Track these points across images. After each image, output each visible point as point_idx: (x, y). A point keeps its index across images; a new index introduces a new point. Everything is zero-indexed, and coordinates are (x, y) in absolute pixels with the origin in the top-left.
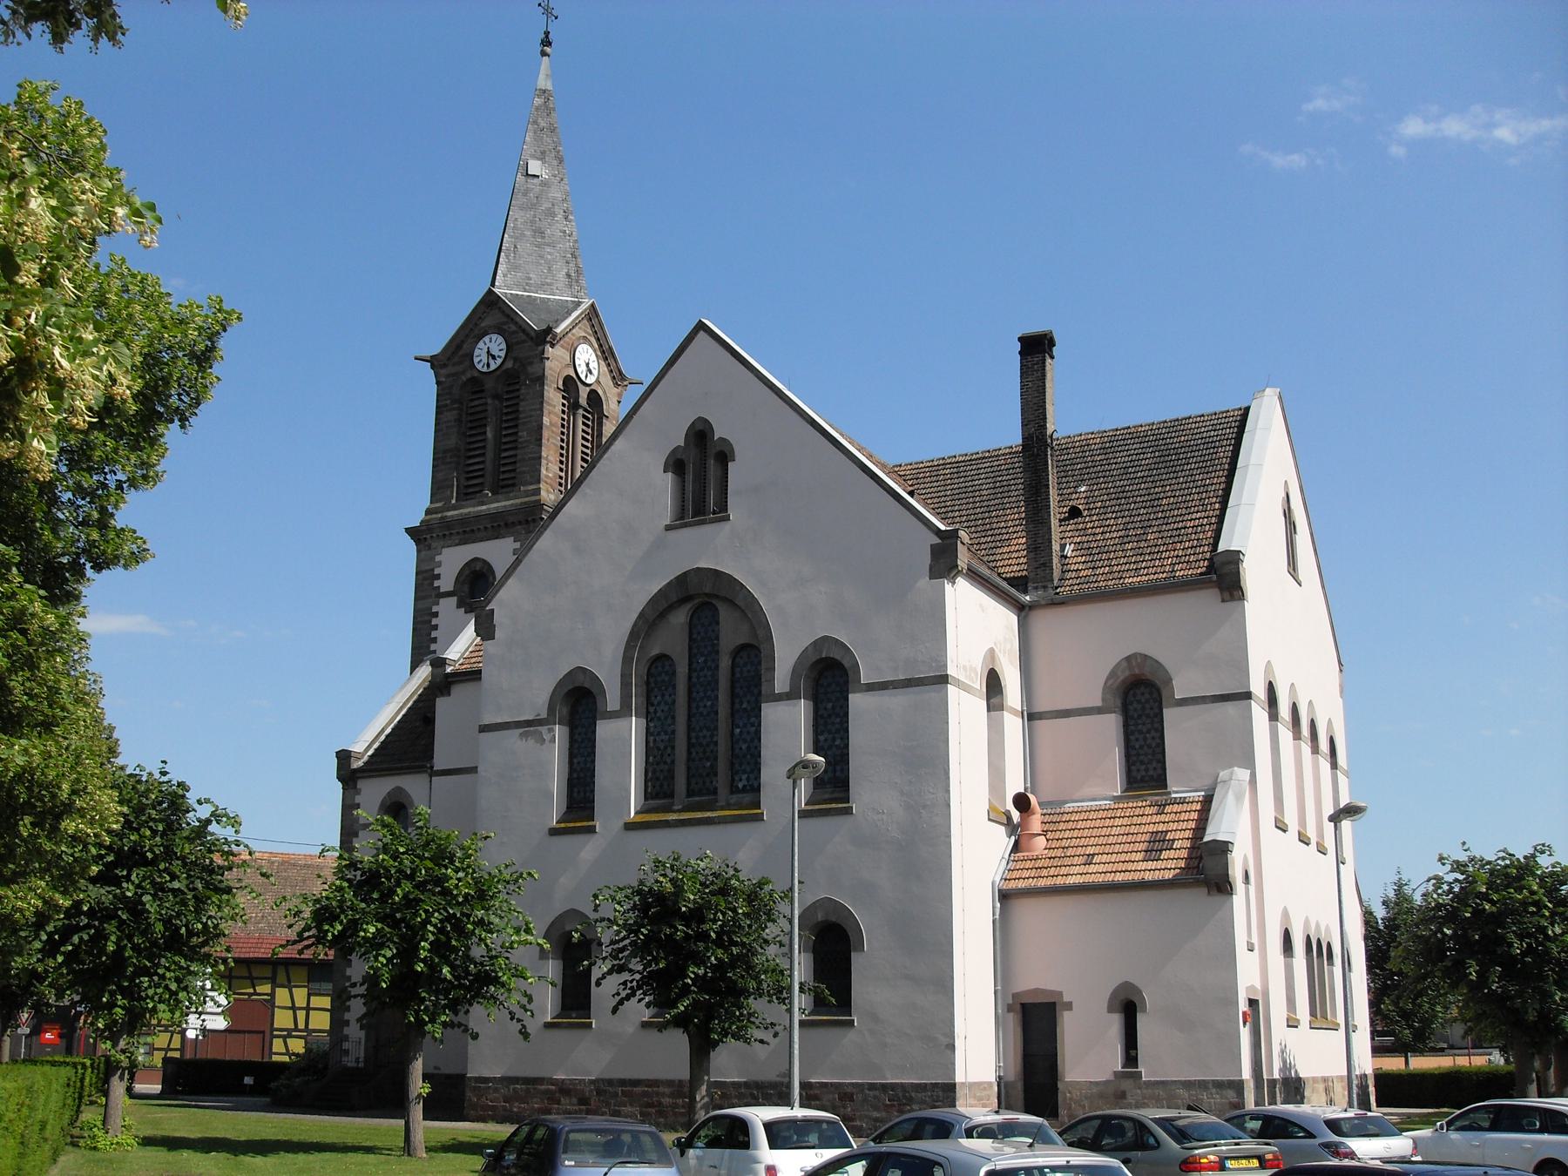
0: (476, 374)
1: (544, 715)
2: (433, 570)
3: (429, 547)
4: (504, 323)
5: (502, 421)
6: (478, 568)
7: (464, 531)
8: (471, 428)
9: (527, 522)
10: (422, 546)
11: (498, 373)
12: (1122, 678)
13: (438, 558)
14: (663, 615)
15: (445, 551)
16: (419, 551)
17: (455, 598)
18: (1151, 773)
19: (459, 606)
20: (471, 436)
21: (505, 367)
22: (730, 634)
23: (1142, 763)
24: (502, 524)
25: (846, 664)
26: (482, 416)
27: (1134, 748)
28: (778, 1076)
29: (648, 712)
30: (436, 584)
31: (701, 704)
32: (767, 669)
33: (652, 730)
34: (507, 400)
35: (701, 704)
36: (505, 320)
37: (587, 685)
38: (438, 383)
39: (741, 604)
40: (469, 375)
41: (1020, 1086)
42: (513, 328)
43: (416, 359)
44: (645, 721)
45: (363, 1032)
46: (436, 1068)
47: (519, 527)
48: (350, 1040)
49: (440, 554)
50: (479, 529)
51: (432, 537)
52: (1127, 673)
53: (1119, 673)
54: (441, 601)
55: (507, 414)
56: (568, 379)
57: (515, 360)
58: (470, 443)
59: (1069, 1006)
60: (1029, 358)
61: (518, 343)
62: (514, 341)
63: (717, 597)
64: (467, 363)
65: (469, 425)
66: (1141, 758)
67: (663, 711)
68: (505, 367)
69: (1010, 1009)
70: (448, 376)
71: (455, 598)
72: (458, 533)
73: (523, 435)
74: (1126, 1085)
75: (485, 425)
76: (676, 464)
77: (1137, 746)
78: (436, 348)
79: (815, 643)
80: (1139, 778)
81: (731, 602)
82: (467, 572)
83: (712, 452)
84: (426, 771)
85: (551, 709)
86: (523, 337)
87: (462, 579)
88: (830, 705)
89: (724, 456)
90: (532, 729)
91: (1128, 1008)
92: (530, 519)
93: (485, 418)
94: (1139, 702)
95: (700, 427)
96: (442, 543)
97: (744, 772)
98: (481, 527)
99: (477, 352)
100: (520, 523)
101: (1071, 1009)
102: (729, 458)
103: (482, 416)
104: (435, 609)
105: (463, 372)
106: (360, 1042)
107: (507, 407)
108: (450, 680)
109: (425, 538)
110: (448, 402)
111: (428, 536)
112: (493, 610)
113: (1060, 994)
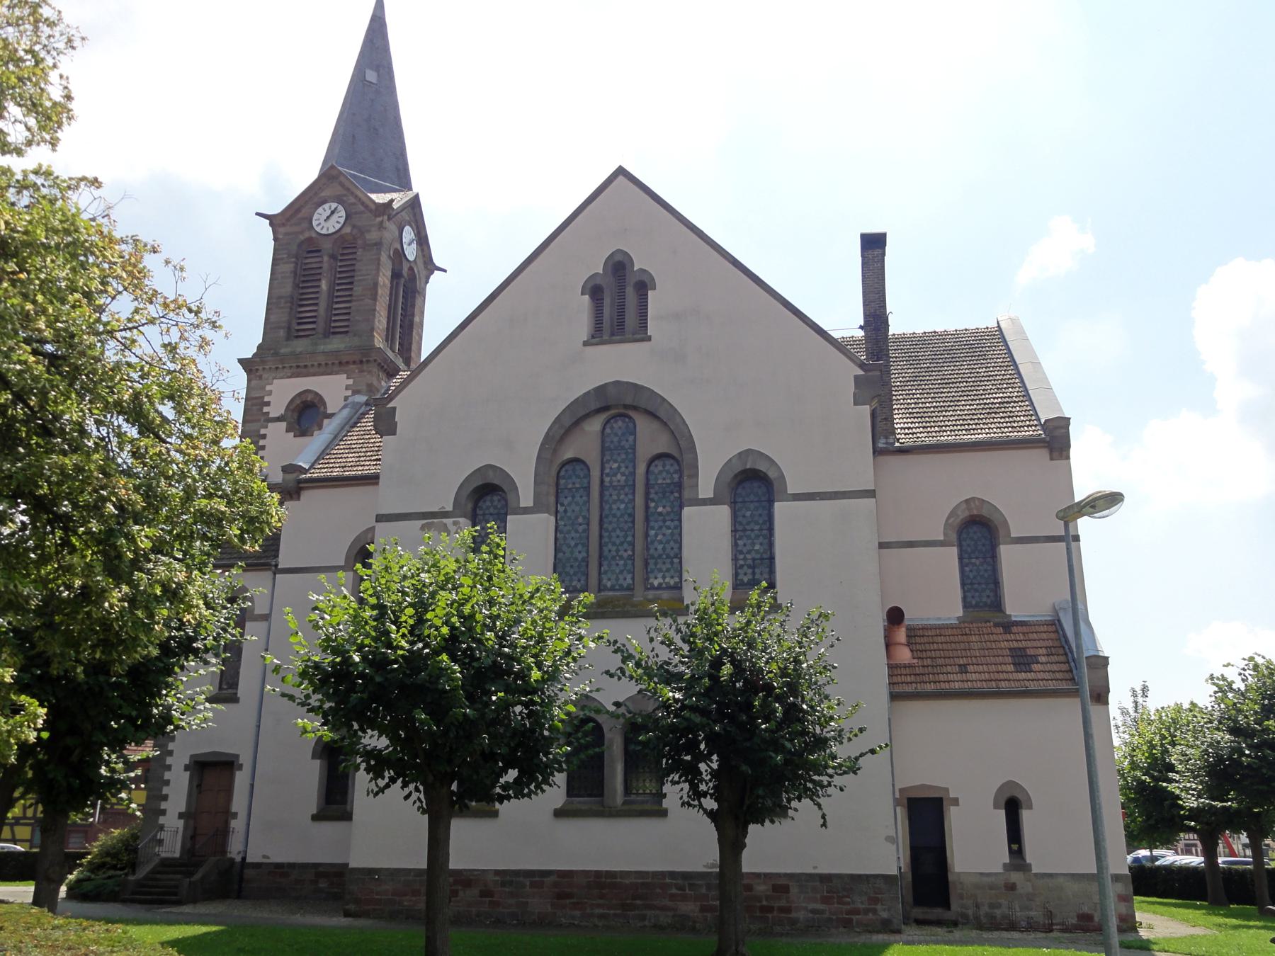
0: (314, 235)
1: (449, 508)
2: (263, 397)
3: (260, 377)
4: (345, 195)
5: (335, 277)
6: (309, 399)
7: (298, 367)
8: (304, 282)
9: (361, 362)
10: (252, 376)
11: (336, 236)
12: (961, 517)
13: (268, 388)
14: (577, 423)
15: (275, 381)
16: (249, 381)
17: (285, 423)
18: (984, 599)
19: (287, 431)
20: (303, 288)
21: (343, 232)
22: (649, 440)
23: (976, 590)
24: (337, 362)
25: (772, 474)
26: (318, 271)
27: (968, 577)
28: (704, 866)
29: (557, 512)
30: (265, 409)
31: (614, 507)
32: (690, 477)
33: (560, 528)
34: (341, 260)
35: (614, 507)
36: (345, 192)
37: (496, 482)
38: (275, 239)
39: (661, 414)
40: (307, 235)
41: (909, 877)
42: (352, 200)
43: (258, 214)
44: (553, 519)
45: (182, 822)
46: (264, 857)
47: (352, 366)
48: (165, 829)
49: (271, 384)
50: (313, 365)
51: (264, 369)
52: (967, 514)
53: (959, 513)
54: (270, 424)
55: (340, 272)
56: (396, 251)
57: (354, 227)
58: (302, 294)
59: (956, 802)
60: (870, 252)
61: (356, 213)
62: (353, 211)
63: (635, 408)
64: (305, 225)
65: (303, 279)
66: (976, 586)
67: (573, 511)
68: (343, 232)
69: (897, 802)
70: (286, 234)
71: (285, 423)
72: (291, 367)
73: (358, 290)
74: (1016, 877)
75: (320, 280)
76: (595, 291)
77: (971, 577)
78: (276, 209)
79: (740, 454)
80: (974, 602)
81: (653, 415)
82: (298, 402)
83: (631, 280)
84: (270, 569)
85: (456, 503)
86: (362, 208)
87: (291, 407)
88: (748, 514)
89: (644, 286)
90: (435, 521)
91: (1013, 807)
92: (364, 360)
93: (320, 274)
94: (972, 539)
95: (618, 258)
96: (274, 375)
97: (660, 570)
98: (316, 364)
99: (316, 216)
100: (354, 362)
101: (958, 805)
102: (649, 287)
103: (318, 271)
104: (263, 432)
105: (302, 232)
106: (177, 832)
107: (340, 267)
108: (301, 485)
109: (257, 370)
110: (285, 256)
111: (261, 368)
112: (394, 409)
113: (947, 790)
